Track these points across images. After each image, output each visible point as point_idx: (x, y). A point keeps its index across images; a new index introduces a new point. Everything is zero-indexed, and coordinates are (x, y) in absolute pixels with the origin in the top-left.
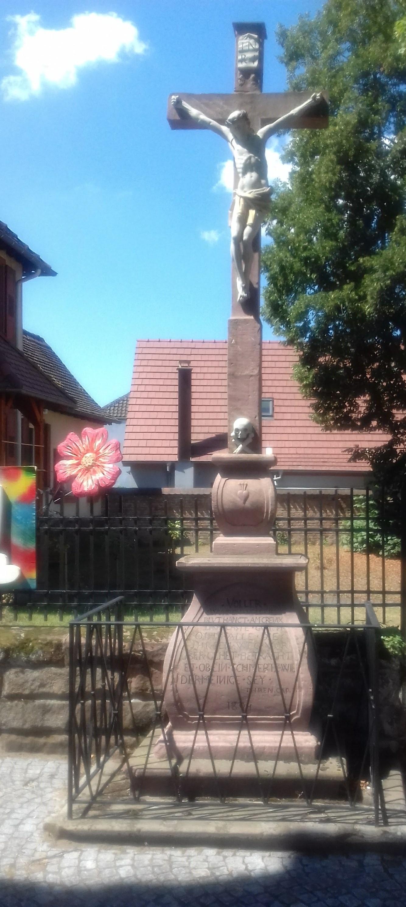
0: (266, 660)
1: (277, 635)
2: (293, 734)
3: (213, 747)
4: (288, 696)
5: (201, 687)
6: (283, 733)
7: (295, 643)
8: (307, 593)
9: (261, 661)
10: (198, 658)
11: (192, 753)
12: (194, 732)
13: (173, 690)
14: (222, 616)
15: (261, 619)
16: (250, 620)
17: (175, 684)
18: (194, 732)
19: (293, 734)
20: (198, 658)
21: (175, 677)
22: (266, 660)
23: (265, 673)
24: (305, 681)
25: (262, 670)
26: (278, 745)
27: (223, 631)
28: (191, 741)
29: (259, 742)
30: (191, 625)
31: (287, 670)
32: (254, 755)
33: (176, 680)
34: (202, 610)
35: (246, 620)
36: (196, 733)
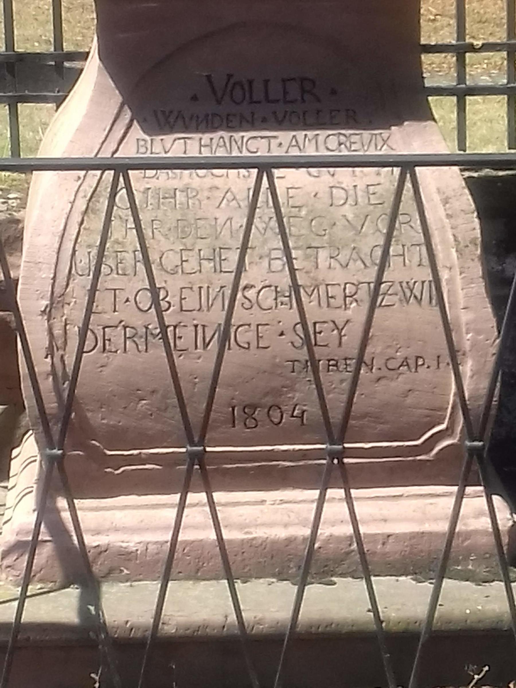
0: (264, 271)
1: (377, 189)
2: (349, 499)
3: (230, 541)
4: (337, 383)
5: (196, 363)
6: (183, 500)
7: (442, 213)
8: (461, 50)
9: (394, 273)
10: (130, 271)
11: (127, 564)
12: (176, 498)
13: (53, 372)
14: (285, 136)
15: (321, 139)
16: (285, 145)
17: (58, 354)
18: (176, 498)
19: (349, 499)
20: (130, 271)
21: (58, 331)
22: (264, 271)
23: (349, 312)
24: (478, 332)
25: (339, 301)
26: (444, 527)
27: (408, 185)
28: (166, 528)
29: (241, 527)
30: (109, 167)
31: (419, 301)
32: (362, 560)
33: (60, 343)
34: (127, 115)
35: (274, 143)
36: (183, 500)
